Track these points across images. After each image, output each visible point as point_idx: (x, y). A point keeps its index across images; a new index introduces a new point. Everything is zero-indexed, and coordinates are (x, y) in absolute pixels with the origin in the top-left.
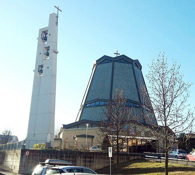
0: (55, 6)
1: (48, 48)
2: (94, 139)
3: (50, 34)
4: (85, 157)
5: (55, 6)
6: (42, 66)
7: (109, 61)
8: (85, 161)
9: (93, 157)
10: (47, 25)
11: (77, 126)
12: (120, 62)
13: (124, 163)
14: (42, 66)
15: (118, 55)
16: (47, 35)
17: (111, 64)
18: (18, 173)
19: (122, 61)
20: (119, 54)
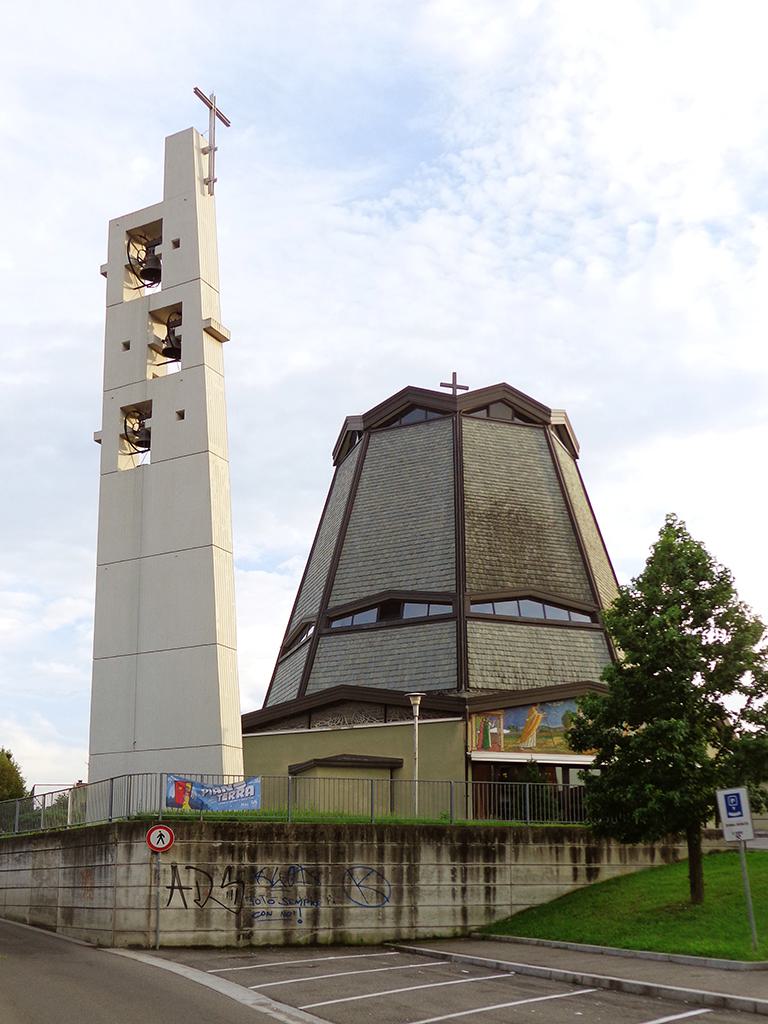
0: (197, 91)
1: (172, 316)
2: (403, 773)
3: (176, 244)
4: (462, 854)
5: (197, 91)
6: (142, 411)
7: (432, 415)
8: (465, 871)
9: (502, 850)
10: (155, 196)
11: (306, 718)
12: (489, 419)
13: (653, 869)
14: (142, 411)
15: (460, 392)
16: (158, 250)
17: (442, 430)
18: (340, 929)
19: (497, 410)
20: (467, 388)
